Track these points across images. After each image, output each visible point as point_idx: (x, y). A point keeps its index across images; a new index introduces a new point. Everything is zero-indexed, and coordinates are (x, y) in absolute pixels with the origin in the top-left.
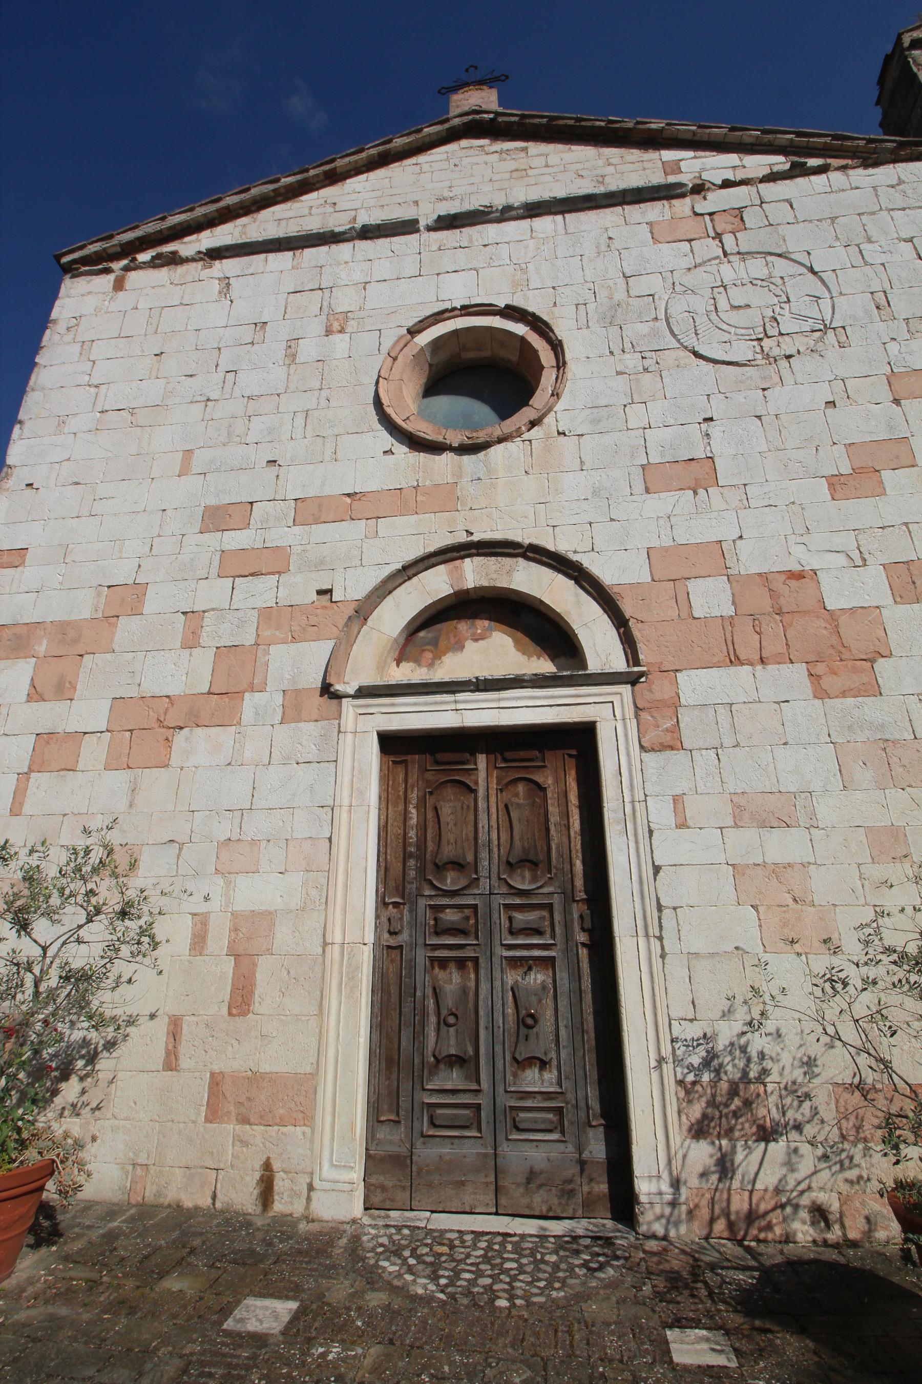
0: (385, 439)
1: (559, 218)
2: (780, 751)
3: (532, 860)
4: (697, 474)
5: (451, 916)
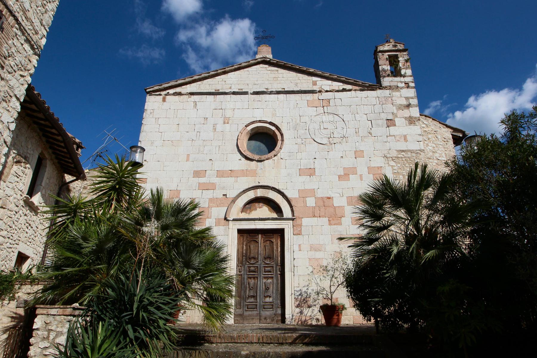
0: (240, 156)
3: (270, 257)
4: (311, 172)
5: (252, 269)
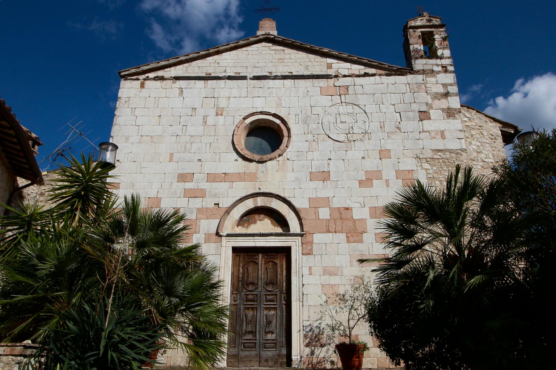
0: (235, 156)
1: (293, 80)
2: (337, 256)
5: (250, 297)
